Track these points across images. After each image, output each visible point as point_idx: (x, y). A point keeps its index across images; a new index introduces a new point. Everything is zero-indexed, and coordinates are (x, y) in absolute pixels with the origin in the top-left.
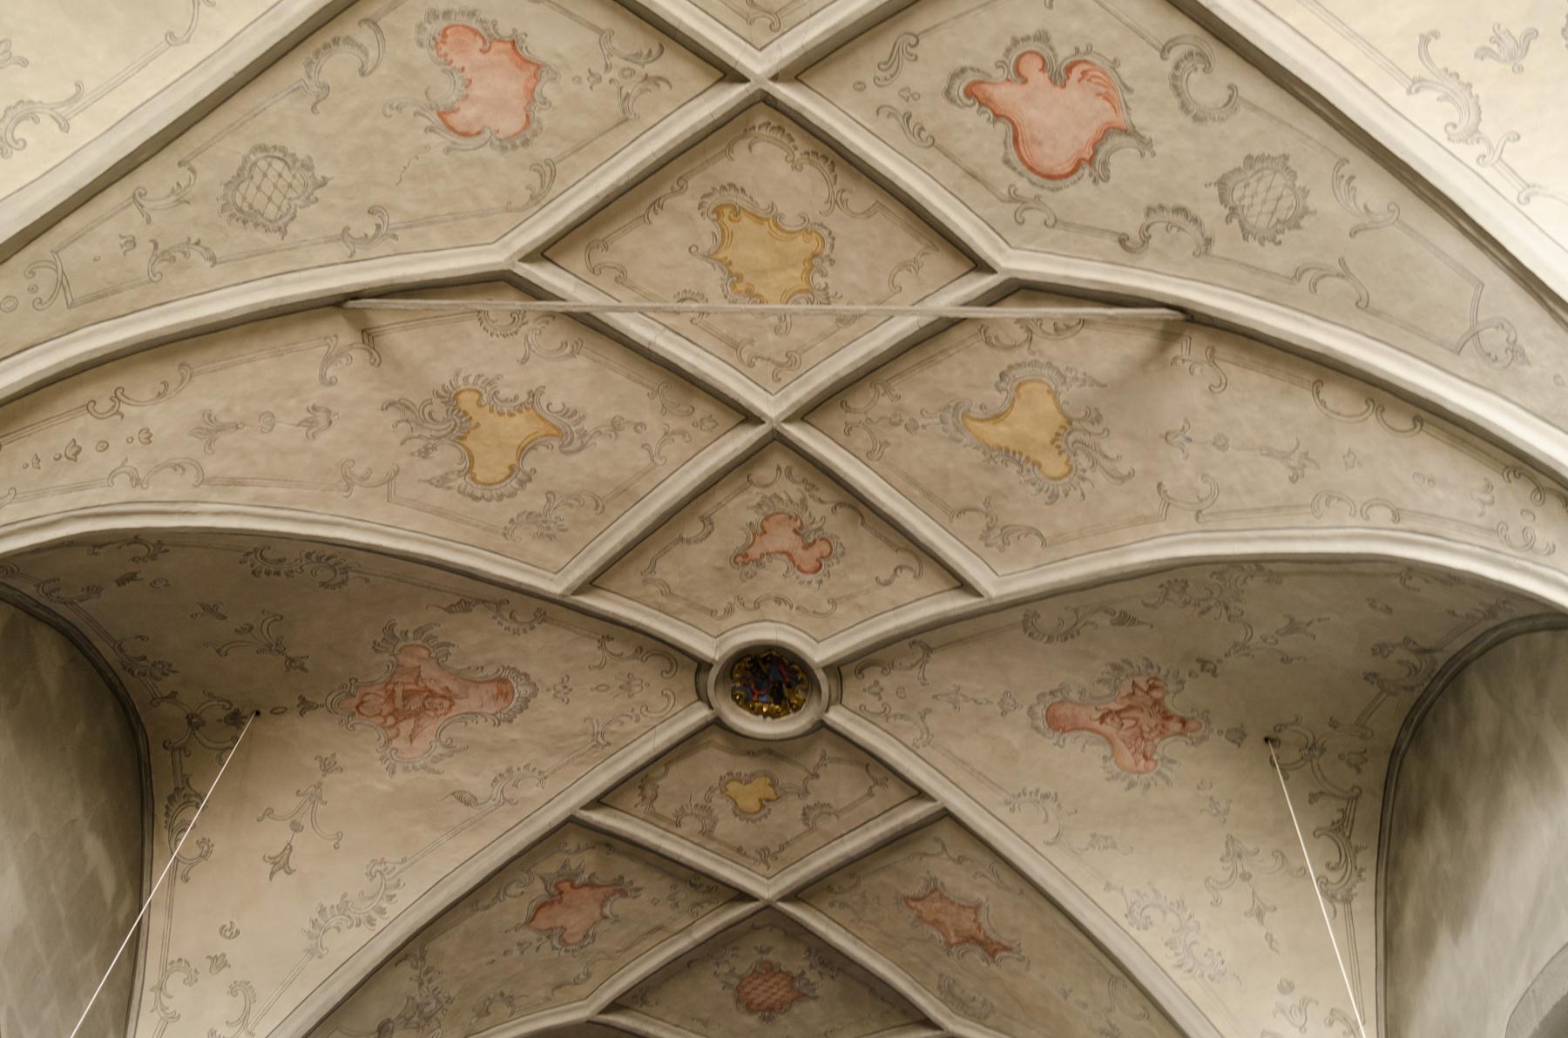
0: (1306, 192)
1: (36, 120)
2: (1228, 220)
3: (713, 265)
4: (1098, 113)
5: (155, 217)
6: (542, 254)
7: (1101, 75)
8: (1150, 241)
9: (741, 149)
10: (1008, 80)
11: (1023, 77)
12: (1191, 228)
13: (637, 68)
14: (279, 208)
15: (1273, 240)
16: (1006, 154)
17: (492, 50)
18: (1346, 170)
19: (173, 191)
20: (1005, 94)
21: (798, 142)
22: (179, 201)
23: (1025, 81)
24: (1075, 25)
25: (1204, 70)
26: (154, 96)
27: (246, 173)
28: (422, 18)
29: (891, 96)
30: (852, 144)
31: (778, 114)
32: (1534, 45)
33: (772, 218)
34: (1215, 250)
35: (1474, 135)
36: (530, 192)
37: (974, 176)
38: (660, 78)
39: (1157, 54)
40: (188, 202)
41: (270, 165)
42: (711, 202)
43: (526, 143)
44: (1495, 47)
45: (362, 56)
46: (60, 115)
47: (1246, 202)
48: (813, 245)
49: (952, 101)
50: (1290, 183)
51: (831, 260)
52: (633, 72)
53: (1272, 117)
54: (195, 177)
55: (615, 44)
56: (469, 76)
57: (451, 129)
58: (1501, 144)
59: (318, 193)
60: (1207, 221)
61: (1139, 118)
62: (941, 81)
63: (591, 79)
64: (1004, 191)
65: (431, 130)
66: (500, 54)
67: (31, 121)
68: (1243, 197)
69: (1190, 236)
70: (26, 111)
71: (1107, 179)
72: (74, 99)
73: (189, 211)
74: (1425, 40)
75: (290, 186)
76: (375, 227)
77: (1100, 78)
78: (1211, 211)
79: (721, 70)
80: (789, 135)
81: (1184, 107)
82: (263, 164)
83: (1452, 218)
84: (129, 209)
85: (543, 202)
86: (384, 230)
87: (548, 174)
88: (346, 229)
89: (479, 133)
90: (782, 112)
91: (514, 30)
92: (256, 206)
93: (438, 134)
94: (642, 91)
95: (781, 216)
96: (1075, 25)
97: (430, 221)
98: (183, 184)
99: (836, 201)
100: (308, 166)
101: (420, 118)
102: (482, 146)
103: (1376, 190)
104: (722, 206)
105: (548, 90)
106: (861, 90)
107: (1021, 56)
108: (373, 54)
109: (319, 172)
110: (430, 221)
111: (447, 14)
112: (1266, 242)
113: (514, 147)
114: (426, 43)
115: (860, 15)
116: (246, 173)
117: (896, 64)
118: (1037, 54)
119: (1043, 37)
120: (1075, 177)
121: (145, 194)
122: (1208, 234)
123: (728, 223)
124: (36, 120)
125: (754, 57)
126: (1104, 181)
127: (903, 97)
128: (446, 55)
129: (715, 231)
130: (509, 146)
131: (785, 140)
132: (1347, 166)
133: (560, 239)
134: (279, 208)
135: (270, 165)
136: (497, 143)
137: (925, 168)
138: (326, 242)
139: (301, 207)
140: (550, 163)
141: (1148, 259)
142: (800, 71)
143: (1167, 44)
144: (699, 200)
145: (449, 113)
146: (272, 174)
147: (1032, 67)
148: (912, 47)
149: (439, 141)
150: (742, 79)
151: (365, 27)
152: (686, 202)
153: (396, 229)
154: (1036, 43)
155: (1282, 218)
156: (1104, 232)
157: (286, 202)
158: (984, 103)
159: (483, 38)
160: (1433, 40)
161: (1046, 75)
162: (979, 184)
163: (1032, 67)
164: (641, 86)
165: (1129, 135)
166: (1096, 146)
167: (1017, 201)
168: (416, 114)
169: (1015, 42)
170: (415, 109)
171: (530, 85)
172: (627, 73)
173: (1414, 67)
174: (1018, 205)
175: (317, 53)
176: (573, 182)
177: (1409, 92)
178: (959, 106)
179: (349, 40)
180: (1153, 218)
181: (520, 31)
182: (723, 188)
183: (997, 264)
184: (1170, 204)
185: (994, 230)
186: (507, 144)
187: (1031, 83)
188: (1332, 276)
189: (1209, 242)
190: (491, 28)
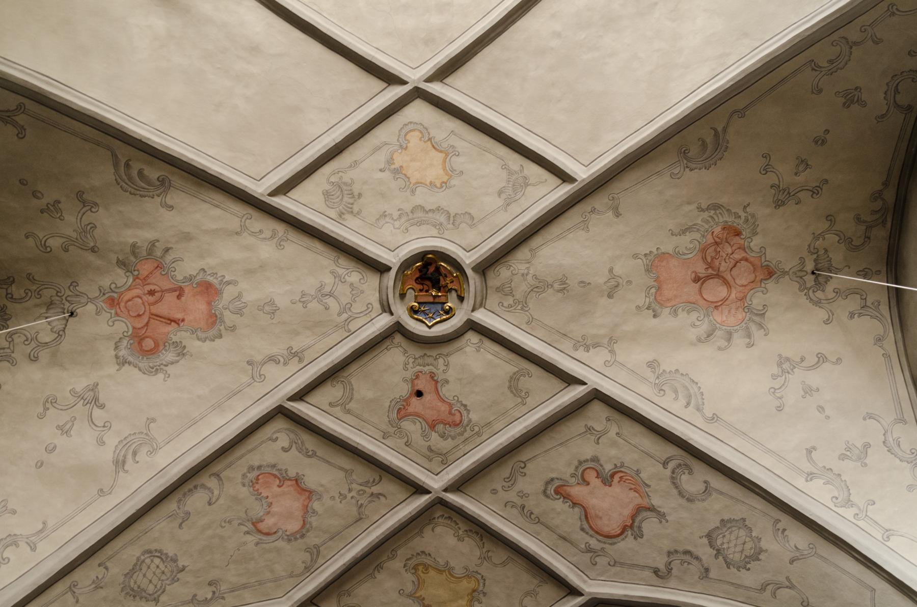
0: (759, 539)
1: (17, 546)
2: (716, 556)
3: (413, 600)
4: (630, 500)
5: (81, 599)
6: (311, 601)
7: (630, 478)
8: (673, 571)
9: (427, 532)
10: (579, 484)
11: (586, 481)
12: (695, 562)
13: (367, 489)
14: (156, 586)
15: (745, 568)
16: (582, 525)
17: (284, 486)
18: (780, 526)
19: (93, 582)
20: (578, 491)
21: (460, 525)
22: (97, 588)
23: (588, 484)
24: (613, 452)
25: (689, 473)
26: (88, 526)
27: (138, 567)
28: (245, 471)
29: (512, 496)
30: (492, 524)
31: (449, 510)
32: (870, 451)
33: (446, 570)
34: (712, 574)
35: (848, 503)
36: (304, 565)
37: (564, 539)
38: (380, 494)
39: (661, 466)
40: (102, 588)
41: (152, 561)
42: (411, 563)
43: (303, 536)
44: (848, 453)
45: (210, 494)
46: (31, 541)
47: (725, 546)
48: (473, 585)
49: (547, 497)
50: (749, 535)
51: (484, 593)
52: (365, 492)
53: (732, 497)
54: (108, 572)
55: (354, 477)
56: (270, 501)
57: (260, 531)
58: (865, 508)
59: (179, 576)
60: (704, 558)
61: (656, 501)
62: (540, 486)
63: (341, 497)
64: (583, 546)
65: (248, 533)
66: (288, 487)
67: (14, 546)
68: (723, 543)
69: (695, 568)
70: (12, 541)
71: (642, 536)
72: (41, 531)
73: (102, 593)
74: (809, 451)
75: (163, 573)
76: (211, 593)
77: (630, 480)
78: (705, 552)
79: (415, 488)
80: (455, 521)
81: (681, 494)
82: (148, 561)
83: (848, 551)
84: (66, 595)
85: (312, 570)
86: (217, 595)
87: (315, 553)
88: (195, 596)
89: (275, 533)
90: (451, 509)
91: (297, 473)
92: (142, 586)
93: (252, 535)
94: (370, 502)
95: (453, 568)
96: (613, 452)
97: (245, 587)
98: (100, 577)
99: (485, 558)
100: (174, 560)
101: (242, 527)
102: (277, 540)
103: (800, 538)
104: (417, 565)
105: (316, 505)
106: (495, 494)
107: (584, 470)
108: (216, 492)
109: (180, 564)
110: (245, 587)
111: (259, 467)
112: (741, 569)
113: (296, 539)
114: (247, 484)
115: (492, 453)
116: (138, 567)
117: (514, 478)
118: (593, 468)
119: (595, 459)
120: (623, 536)
121: (77, 585)
122: (706, 565)
123: (422, 575)
124: (17, 546)
125: (433, 479)
126: (640, 537)
127: (519, 496)
128: (258, 490)
129: (414, 579)
130: (292, 538)
131: (453, 524)
132: (780, 523)
133: (322, 592)
134: (156, 586)
135: (152, 561)
136: (286, 537)
137: (535, 536)
138: (182, 605)
139: (168, 585)
140: (317, 547)
141: (673, 583)
142: (460, 485)
143: (666, 460)
144: (404, 563)
145: (259, 522)
146: (153, 566)
147: (591, 476)
148: (522, 468)
149: (251, 539)
150: (428, 492)
151: (213, 478)
152: (397, 564)
153: (224, 593)
154: (592, 463)
155: (748, 554)
156: (643, 567)
157: (160, 582)
158: (566, 497)
159: (279, 478)
160: (814, 451)
161: (600, 480)
162: (569, 544)
163: (591, 476)
164: (369, 499)
165: (651, 511)
166: (633, 517)
167: (590, 552)
168: (240, 524)
169: (580, 463)
170: (239, 522)
171: (306, 503)
172: (361, 493)
173: (807, 467)
174: (592, 554)
175: (185, 495)
176: (330, 556)
177: (807, 481)
178: (552, 499)
179: (203, 486)
180: (672, 558)
181: (300, 474)
182: (418, 554)
183: (584, 590)
184: (681, 549)
185: (580, 570)
186: (291, 538)
187: (592, 485)
188: (784, 587)
189: (707, 570)
190: (284, 473)
